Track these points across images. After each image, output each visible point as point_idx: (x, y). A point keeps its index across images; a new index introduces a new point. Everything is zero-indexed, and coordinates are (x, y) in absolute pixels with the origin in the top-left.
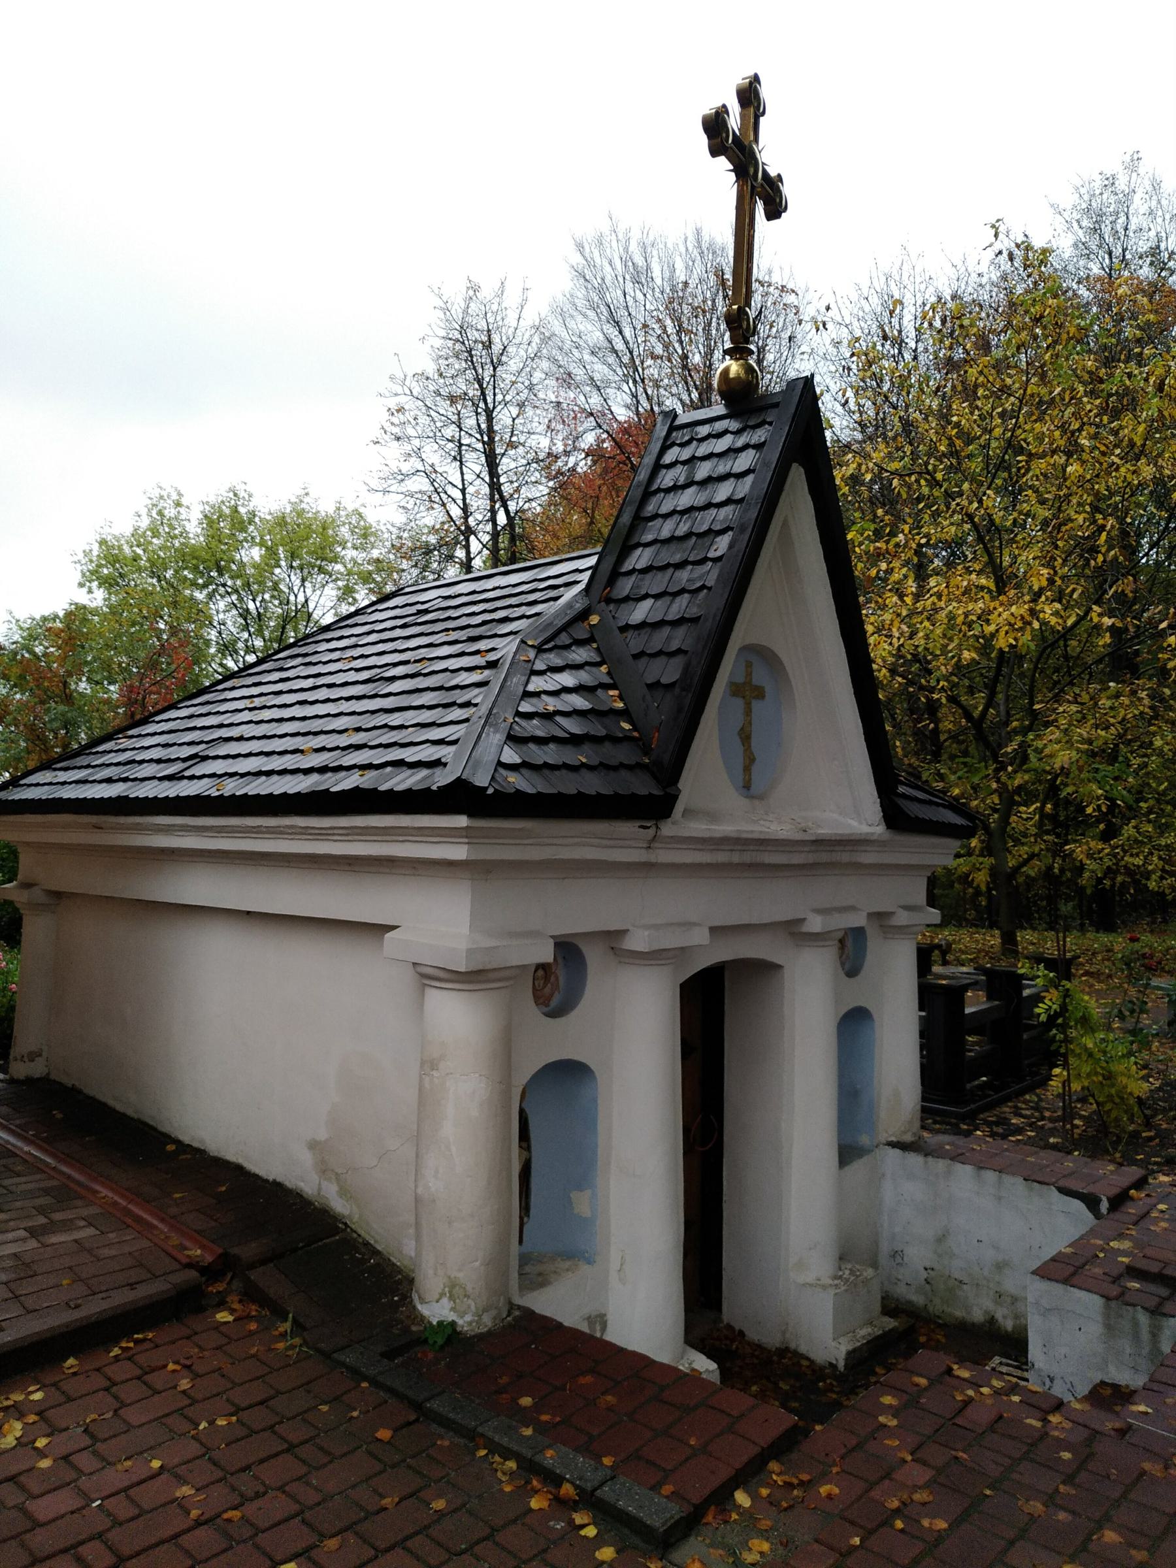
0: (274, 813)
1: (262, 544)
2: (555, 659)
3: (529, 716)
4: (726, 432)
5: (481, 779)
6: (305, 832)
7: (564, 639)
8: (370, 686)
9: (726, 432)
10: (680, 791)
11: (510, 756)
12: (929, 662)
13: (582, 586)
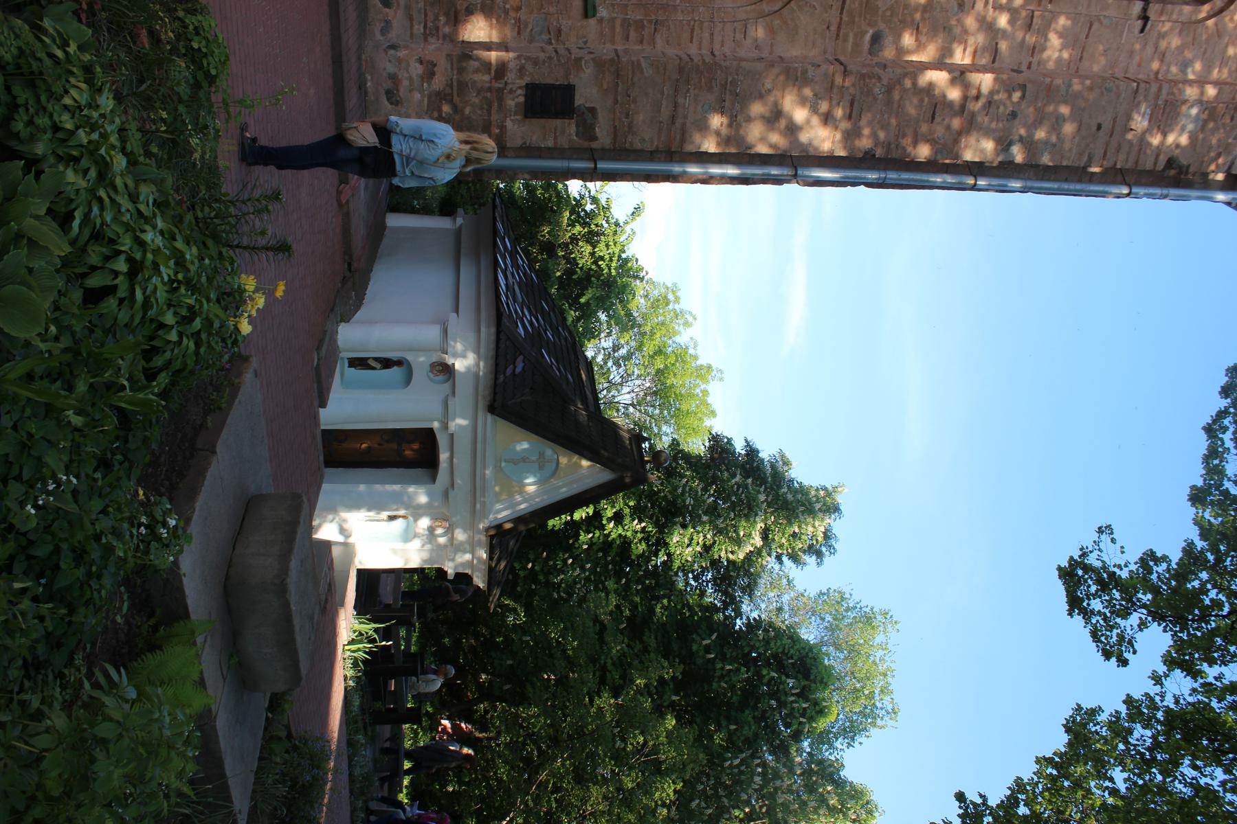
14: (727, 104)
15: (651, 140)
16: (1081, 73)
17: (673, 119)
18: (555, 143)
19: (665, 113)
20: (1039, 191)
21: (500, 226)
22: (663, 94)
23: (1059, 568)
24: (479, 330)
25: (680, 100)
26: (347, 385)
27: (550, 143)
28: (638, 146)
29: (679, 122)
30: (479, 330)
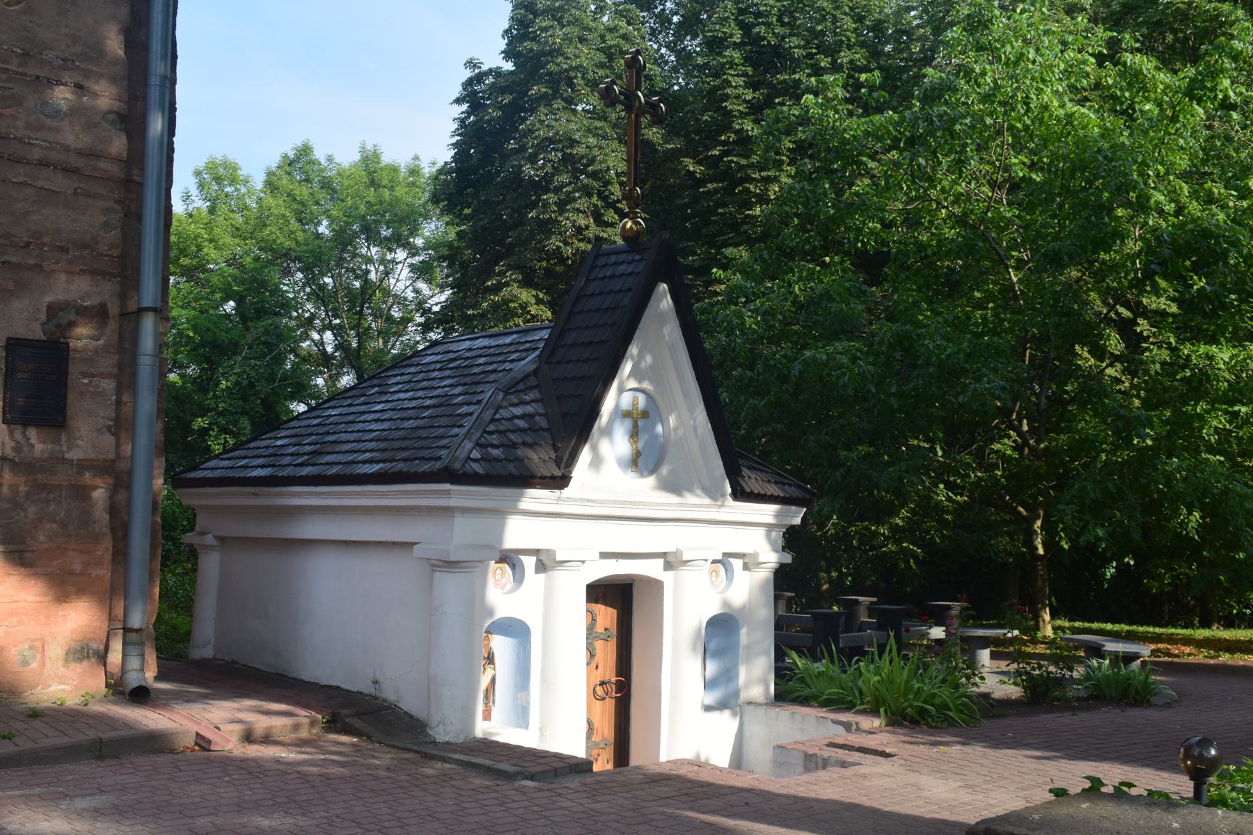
0: (242, 485)
1: (862, 44)
2: (514, 399)
3: (491, 433)
4: (623, 262)
5: (457, 465)
6: (374, 494)
7: (521, 387)
8: (440, 409)
9: (623, 262)
10: (642, 476)
11: (475, 454)
12: (1223, 334)
13: (537, 352)
14: (43, 73)
15: (107, 210)
16: (159, 304)
17: (70, 171)
18: (109, 376)
19: (60, 182)
20: (170, 81)
21: (447, 766)
22: (24, 184)
23: (305, 151)
24: (449, 511)
25: (36, 154)
26: (521, 716)
27: (108, 385)
28: (115, 234)
29: (75, 161)
30: (449, 511)
